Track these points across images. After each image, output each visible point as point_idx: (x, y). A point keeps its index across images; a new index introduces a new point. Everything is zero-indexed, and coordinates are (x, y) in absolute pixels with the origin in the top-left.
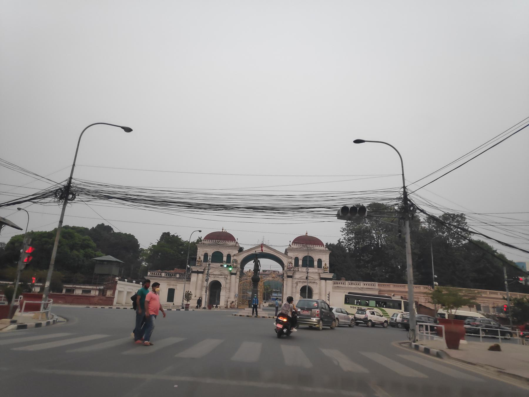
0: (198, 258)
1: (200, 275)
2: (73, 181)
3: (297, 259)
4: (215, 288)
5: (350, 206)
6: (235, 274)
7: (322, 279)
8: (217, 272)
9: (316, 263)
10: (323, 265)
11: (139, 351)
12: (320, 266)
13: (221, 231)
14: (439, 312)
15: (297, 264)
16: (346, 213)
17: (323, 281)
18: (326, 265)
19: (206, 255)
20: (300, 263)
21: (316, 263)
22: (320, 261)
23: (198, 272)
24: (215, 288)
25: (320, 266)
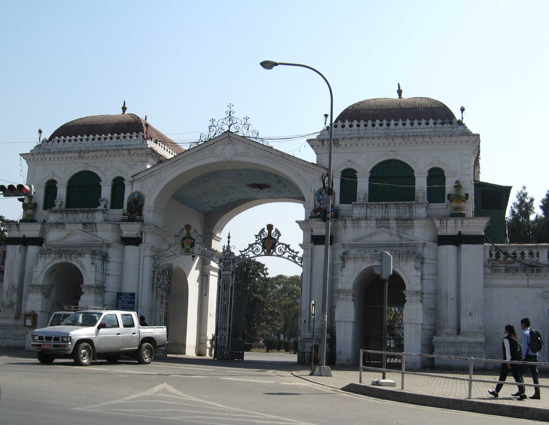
1: (32, 250)
10: (449, 187)
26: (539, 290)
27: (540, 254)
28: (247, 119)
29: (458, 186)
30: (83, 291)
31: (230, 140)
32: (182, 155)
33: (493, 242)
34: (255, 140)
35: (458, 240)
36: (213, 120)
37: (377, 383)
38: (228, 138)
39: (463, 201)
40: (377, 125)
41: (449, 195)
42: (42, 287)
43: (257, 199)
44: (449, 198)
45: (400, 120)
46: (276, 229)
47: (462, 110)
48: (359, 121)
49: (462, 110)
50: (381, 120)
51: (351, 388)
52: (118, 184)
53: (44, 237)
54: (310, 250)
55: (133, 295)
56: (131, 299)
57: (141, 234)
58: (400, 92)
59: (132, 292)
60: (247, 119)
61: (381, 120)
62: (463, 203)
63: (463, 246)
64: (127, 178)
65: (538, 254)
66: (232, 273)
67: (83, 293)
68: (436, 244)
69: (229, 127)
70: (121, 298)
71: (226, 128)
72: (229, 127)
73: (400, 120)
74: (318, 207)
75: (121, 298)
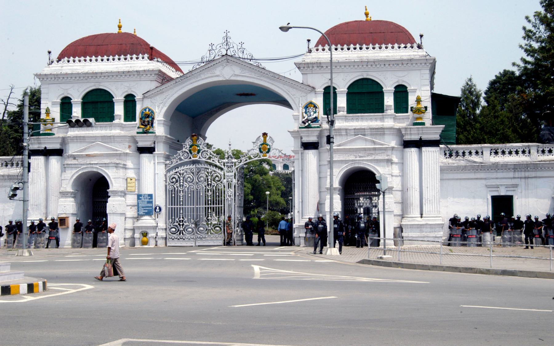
0: (43, 111)
1: (54, 160)
2: (333, 59)
3: (329, 94)
4: (95, 191)
5: (405, 58)
6: (150, 150)
7: (407, 144)
8: (101, 146)
9: (389, 100)
10: (412, 101)
11: (45, 280)
12: (401, 104)
13: (115, 31)
14: (486, 104)
15: (330, 108)
16: (292, 218)
17: (413, 152)
18: (418, 101)
19: (66, 104)
20: (342, 102)
21: (389, 100)
22: (401, 92)
23: (47, 153)
24: (95, 191)
25: (401, 104)
26: (484, 182)
27: (484, 153)
28: (242, 43)
29: (418, 101)
30: (109, 195)
31: (228, 62)
32: (185, 77)
33: (446, 143)
34: (248, 61)
35: (419, 144)
36: (212, 45)
37: (381, 258)
38: (226, 61)
39: (424, 113)
40: (352, 49)
41: (412, 108)
42: (72, 193)
43: (239, 103)
44: (412, 110)
45: (371, 45)
46: (270, 137)
47: (421, 36)
48: (336, 45)
49: (421, 36)
50: (355, 45)
51: (363, 262)
52: (130, 101)
53: (64, 149)
54: (300, 154)
55: (151, 196)
56: (150, 199)
57: (154, 143)
58: (367, 15)
59: (150, 193)
60: (242, 43)
61: (355, 45)
62: (423, 114)
63: (424, 149)
64: (138, 97)
65: (482, 152)
66: (235, 174)
67: (109, 197)
68: (402, 147)
69: (227, 51)
70: (141, 199)
71: (224, 53)
72: (227, 51)
73: (371, 45)
74: (306, 118)
75: (141, 199)
